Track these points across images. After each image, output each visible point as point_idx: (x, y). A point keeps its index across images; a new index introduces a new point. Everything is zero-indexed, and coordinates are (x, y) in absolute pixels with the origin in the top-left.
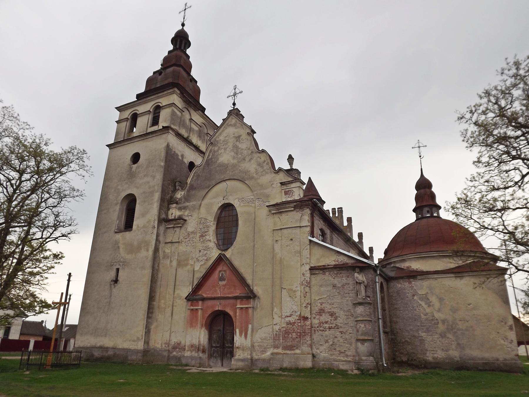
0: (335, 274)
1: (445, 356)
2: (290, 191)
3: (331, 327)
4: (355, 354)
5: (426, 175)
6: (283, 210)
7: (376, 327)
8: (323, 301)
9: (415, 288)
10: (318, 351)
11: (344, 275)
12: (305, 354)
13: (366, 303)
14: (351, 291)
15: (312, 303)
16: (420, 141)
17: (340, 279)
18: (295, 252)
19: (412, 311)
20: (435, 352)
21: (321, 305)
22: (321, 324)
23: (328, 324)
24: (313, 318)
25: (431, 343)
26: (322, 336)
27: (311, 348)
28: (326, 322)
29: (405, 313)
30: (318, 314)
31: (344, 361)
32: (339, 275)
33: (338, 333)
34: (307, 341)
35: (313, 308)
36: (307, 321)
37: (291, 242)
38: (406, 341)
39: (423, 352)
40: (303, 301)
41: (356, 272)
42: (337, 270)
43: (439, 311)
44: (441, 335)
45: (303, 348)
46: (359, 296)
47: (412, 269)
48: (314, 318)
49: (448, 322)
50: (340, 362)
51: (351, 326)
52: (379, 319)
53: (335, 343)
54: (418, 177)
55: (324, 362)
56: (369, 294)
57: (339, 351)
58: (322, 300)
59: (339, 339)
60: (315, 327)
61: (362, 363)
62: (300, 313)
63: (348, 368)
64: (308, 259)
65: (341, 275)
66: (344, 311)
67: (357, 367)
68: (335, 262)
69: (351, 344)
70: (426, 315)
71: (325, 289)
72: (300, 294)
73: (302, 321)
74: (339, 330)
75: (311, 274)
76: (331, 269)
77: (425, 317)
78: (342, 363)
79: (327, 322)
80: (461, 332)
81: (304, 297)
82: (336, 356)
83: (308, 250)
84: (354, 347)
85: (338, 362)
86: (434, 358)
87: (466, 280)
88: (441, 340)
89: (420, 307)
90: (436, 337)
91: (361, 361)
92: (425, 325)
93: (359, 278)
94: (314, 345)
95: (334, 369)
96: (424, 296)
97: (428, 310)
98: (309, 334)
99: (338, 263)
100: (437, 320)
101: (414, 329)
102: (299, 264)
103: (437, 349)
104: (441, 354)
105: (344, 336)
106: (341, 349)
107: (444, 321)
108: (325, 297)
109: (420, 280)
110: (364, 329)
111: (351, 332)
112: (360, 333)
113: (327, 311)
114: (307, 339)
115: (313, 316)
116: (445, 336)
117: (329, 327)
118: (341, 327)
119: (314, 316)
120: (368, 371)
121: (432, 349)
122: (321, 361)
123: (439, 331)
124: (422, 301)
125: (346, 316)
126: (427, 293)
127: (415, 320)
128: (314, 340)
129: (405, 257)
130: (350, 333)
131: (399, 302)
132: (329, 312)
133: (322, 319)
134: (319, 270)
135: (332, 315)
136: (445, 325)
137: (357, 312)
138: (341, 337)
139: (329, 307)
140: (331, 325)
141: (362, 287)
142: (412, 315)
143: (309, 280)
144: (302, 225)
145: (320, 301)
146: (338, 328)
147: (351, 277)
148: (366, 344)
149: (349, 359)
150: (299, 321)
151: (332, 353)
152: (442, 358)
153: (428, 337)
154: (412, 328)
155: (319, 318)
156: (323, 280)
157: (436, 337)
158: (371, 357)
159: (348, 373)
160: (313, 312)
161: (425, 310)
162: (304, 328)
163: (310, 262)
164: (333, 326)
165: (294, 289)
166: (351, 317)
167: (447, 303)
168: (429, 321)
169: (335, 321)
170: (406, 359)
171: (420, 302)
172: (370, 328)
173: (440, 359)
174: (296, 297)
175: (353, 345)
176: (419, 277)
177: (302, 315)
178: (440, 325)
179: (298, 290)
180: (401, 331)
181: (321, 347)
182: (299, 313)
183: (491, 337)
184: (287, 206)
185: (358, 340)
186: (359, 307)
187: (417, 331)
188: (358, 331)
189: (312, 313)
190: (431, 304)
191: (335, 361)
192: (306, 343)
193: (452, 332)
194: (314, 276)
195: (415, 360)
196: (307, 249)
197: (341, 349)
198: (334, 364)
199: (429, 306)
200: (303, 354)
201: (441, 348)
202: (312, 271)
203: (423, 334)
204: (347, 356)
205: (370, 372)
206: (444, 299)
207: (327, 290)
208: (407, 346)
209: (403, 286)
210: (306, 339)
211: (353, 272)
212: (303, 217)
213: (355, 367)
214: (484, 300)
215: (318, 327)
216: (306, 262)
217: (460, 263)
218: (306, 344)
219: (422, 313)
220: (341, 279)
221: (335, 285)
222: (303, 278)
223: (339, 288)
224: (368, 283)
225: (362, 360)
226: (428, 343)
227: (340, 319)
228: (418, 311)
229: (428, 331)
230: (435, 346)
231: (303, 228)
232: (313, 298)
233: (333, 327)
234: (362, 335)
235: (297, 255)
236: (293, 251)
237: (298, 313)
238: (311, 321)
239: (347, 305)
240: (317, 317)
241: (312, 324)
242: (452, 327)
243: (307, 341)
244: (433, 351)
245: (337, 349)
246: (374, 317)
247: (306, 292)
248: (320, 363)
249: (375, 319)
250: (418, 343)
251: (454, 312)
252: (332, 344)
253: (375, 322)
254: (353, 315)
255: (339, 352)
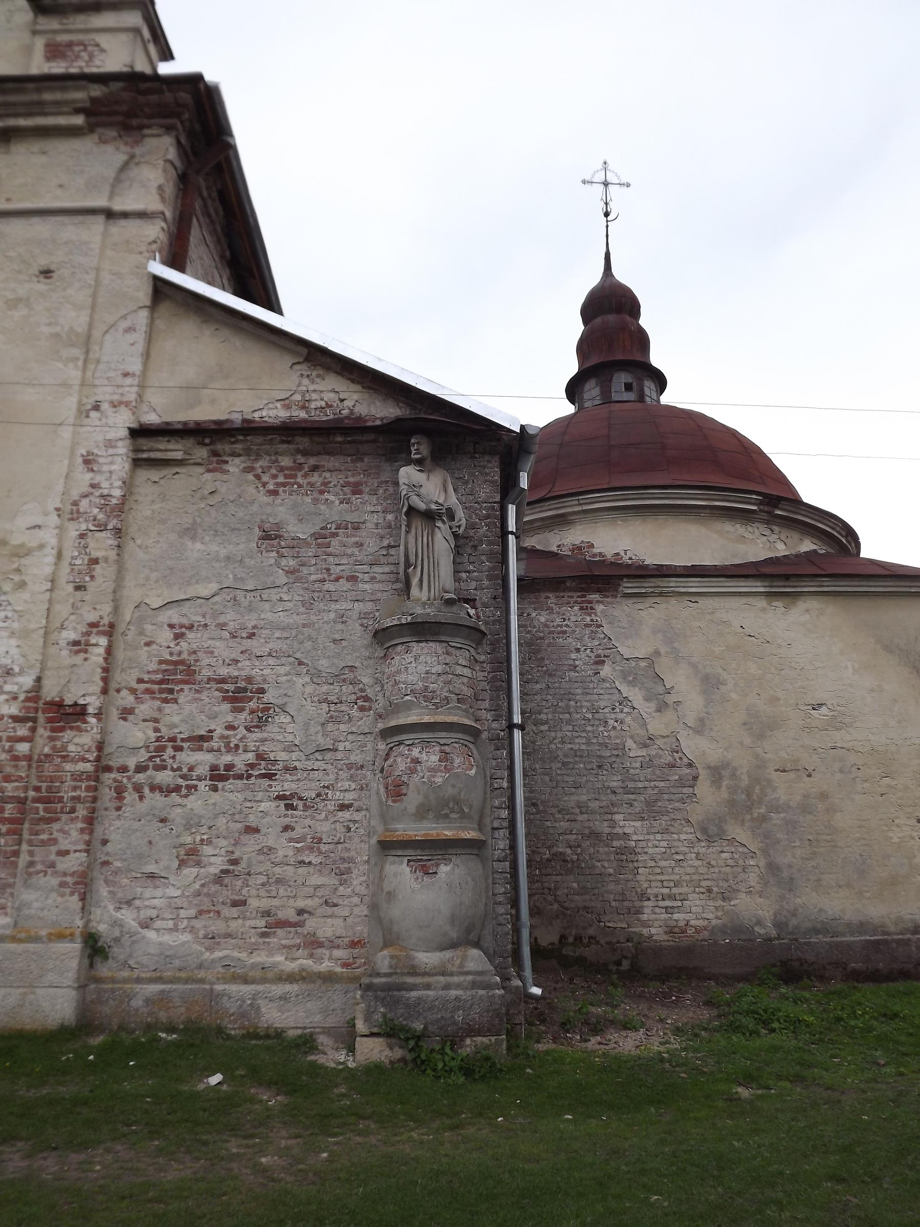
0: (282, 469)
1: (717, 918)
2: (81, 43)
3: (229, 767)
4: (361, 930)
5: (621, 274)
6: (22, 122)
7: (499, 773)
8: (193, 614)
9: (607, 629)
10: (128, 917)
11: (334, 479)
12: (37, 939)
13: (456, 628)
14: (366, 568)
15: (121, 627)
16: (611, 166)
17: (308, 500)
18: (57, 336)
19: (589, 728)
20: (679, 904)
21: (178, 637)
22: (162, 749)
23: (211, 750)
24: (115, 713)
25: (663, 863)
26: (163, 820)
27: (83, 899)
28: (200, 741)
29: (559, 734)
30: (148, 691)
31: (291, 978)
32: (305, 476)
33: (264, 806)
34: (64, 853)
35: (121, 655)
36: (79, 729)
37: (42, 286)
38: (555, 855)
39: (626, 904)
40: (62, 610)
41: (409, 462)
42: (298, 451)
43: (700, 727)
44: (704, 830)
45: (28, 896)
46: (415, 591)
47: (595, 555)
48: (125, 713)
49: (733, 776)
50: (263, 981)
51: (350, 766)
52: (511, 726)
53: (243, 864)
54: (594, 278)
55: (163, 987)
56: (473, 584)
57: (267, 913)
58: (186, 608)
59: (271, 843)
60: (123, 769)
61: (414, 994)
62: (39, 679)
63: (318, 1018)
64: (129, 381)
65: (316, 478)
66: (315, 676)
67: (386, 1021)
68: (288, 407)
69: (343, 874)
70: (645, 746)
71: (214, 547)
72: (48, 570)
73: (43, 732)
74: (277, 788)
75: (137, 463)
76: (259, 439)
77: (640, 753)
78: (279, 989)
79: (202, 738)
80: (782, 815)
81: (78, 588)
82: (240, 948)
83: (139, 337)
84: (362, 890)
85: (253, 982)
86: (670, 931)
87: (807, 611)
88: (702, 850)
89: (622, 712)
90: (683, 837)
91: (410, 980)
92: (640, 785)
93: (423, 491)
94: (106, 882)
95: (220, 1030)
96: (643, 664)
97: (656, 726)
98: (81, 812)
99: (303, 415)
100: (690, 765)
101: (594, 805)
102: (72, 402)
103: (684, 890)
104: (699, 910)
105: (303, 823)
106: (276, 902)
107: (717, 773)
108: (205, 593)
109: (630, 601)
110: (439, 780)
111: (349, 797)
112: (412, 801)
113: (206, 673)
114: (64, 844)
115: (121, 703)
116: (721, 833)
117: (214, 768)
118: (287, 769)
119: (128, 699)
120: (454, 1041)
121: (666, 891)
122: (138, 980)
123: (696, 813)
124: (633, 683)
125: (325, 706)
126: (657, 653)
127: (600, 767)
128: (109, 847)
129: (571, 506)
130: (343, 807)
131: (538, 686)
132: (223, 681)
133: (176, 719)
134: (189, 442)
135: (241, 700)
136: (724, 789)
137: (402, 677)
138: (286, 828)
139: (223, 649)
140: (227, 758)
141: (438, 536)
142: (589, 743)
143: (117, 493)
144: (117, 206)
145: (173, 615)
146: (269, 776)
147: (374, 493)
148: (444, 869)
149: (325, 966)
150: (22, 731)
151: (218, 926)
152: (705, 928)
153: (652, 837)
154: (584, 798)
155: (156, 715)
156: (203, 498)
157: (683, 837)
158: (475, 952)
159: (321, 1059)
160: (118, 678)
161: (644, 725)
162: (48, 769)
163: (140, 396)
164: (240, 761)
165: (15, 540)
166: (355, 712)
167: (734, 696)
168: (658, 772)
169: (256, 735)
170: (555, 938)
171: (625, 690)
172: (473, 772)
173: (698, 930)
174: (22, 585)
175: (358, 880)
176: (628, 586)
177: (50, 691)
178: (703, 789)
179: (41, 546)
180: (538, 812)
181: (148, 893)
182: (27, 681)
183: (895, 837)
184: (48, 96)
185: (387, 846)
186: (416, 648)
187: (608, 811)
188: (396, 791)
189: (113, 685)
190: (670, 699)
191: (236, 979)
192: (52, 865)
193: (748, 817)
194: (155, 474)
195: (591, 938)
196: (130, 330)
197: (276, 902)
198: (223, 994)
199: (662, 707)
200: (20, 941)
201: (704, 884)
202: (144, 443)
203: (630, 827)
204: (313, 944)
205: (469, 1046)
206: (720, 682)
207: (223, 552)
208: (559, 878)
209: (558, 621)
210: (54, 841)
211: (386, 466)
212: (134, 172)
213: (367, 1019)
214: (872, 690)
215: (140, 769)
216: (116, 398)
217: (781, 550)
218: (55, 873)
219: (632, 737)
220: (316, 501)
221: (278, 526)
222: (84, 478)
223: (297, 544)
224: (471, 526)
225: (414, 971)
226: (652, 864)
227: (286, 719)
228: (614, 728)
229: (651, 811)
230: (677, 878)
231: (123, 222)
232: (132, 593)
233: (240, 767)
234: (422, 813)
235: (67, 352)
236: (46, 330)
237: (20, 679)
238: (103, 732)
239: (335, 641)
240: (146, 708)
241: (107, 750)
242: (749, 795)
243: (64, 853)
244: (672, 897)
245: (253, 903)
246: (489, 716)
247: (95, 561)
248: (130, 997)
249: (495, 725)
250: (606, 865)
251: (761, 736)
252: (223, 871)
253: (495, 739)
254: (367, 699)
255: (261, 923)
